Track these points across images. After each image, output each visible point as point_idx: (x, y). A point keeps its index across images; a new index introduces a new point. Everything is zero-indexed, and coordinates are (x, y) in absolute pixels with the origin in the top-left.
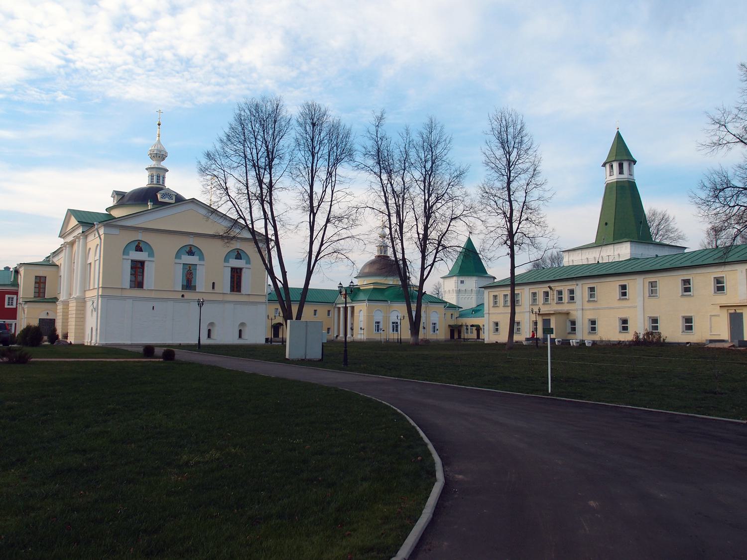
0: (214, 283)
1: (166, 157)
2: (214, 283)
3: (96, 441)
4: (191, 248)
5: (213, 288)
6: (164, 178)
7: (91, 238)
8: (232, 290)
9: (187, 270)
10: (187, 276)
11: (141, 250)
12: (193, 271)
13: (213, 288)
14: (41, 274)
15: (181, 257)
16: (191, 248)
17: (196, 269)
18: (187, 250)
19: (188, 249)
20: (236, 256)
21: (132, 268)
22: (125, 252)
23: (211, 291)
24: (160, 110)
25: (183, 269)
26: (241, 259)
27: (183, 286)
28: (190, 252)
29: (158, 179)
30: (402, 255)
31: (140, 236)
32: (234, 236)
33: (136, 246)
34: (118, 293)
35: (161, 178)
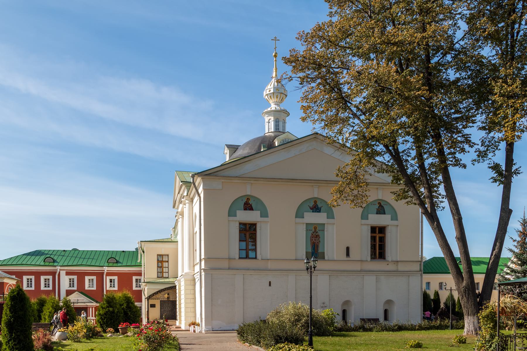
0: (348, 249)
2: (348, 249)
3: (388, 169)
4: (315, 202)
5: (348, 254)
6: (284, 122)
7: (515, 259)
8: (373, 256)
9: (311, 232)
10: (311, 240)
11: (251, 209)
12: (320, 233)
13: (348, 254)
15: (303, 214)
16: (315, 202)
17: (323, 230)
18: (311, 206)
19: (312, 204)
20: (377, 209)
21: (240, 231)
22: (231, 213)
23: (344, 257)
24: (275, 38)
25: (307, 230)
26: (385, 214)
27: (307, 253)
28: (315, 207)
30: (66, 265)
31: (248, 190)
32: (277, 342)
33: (245, 204)
34: (226, 264)
35: (281, 124)
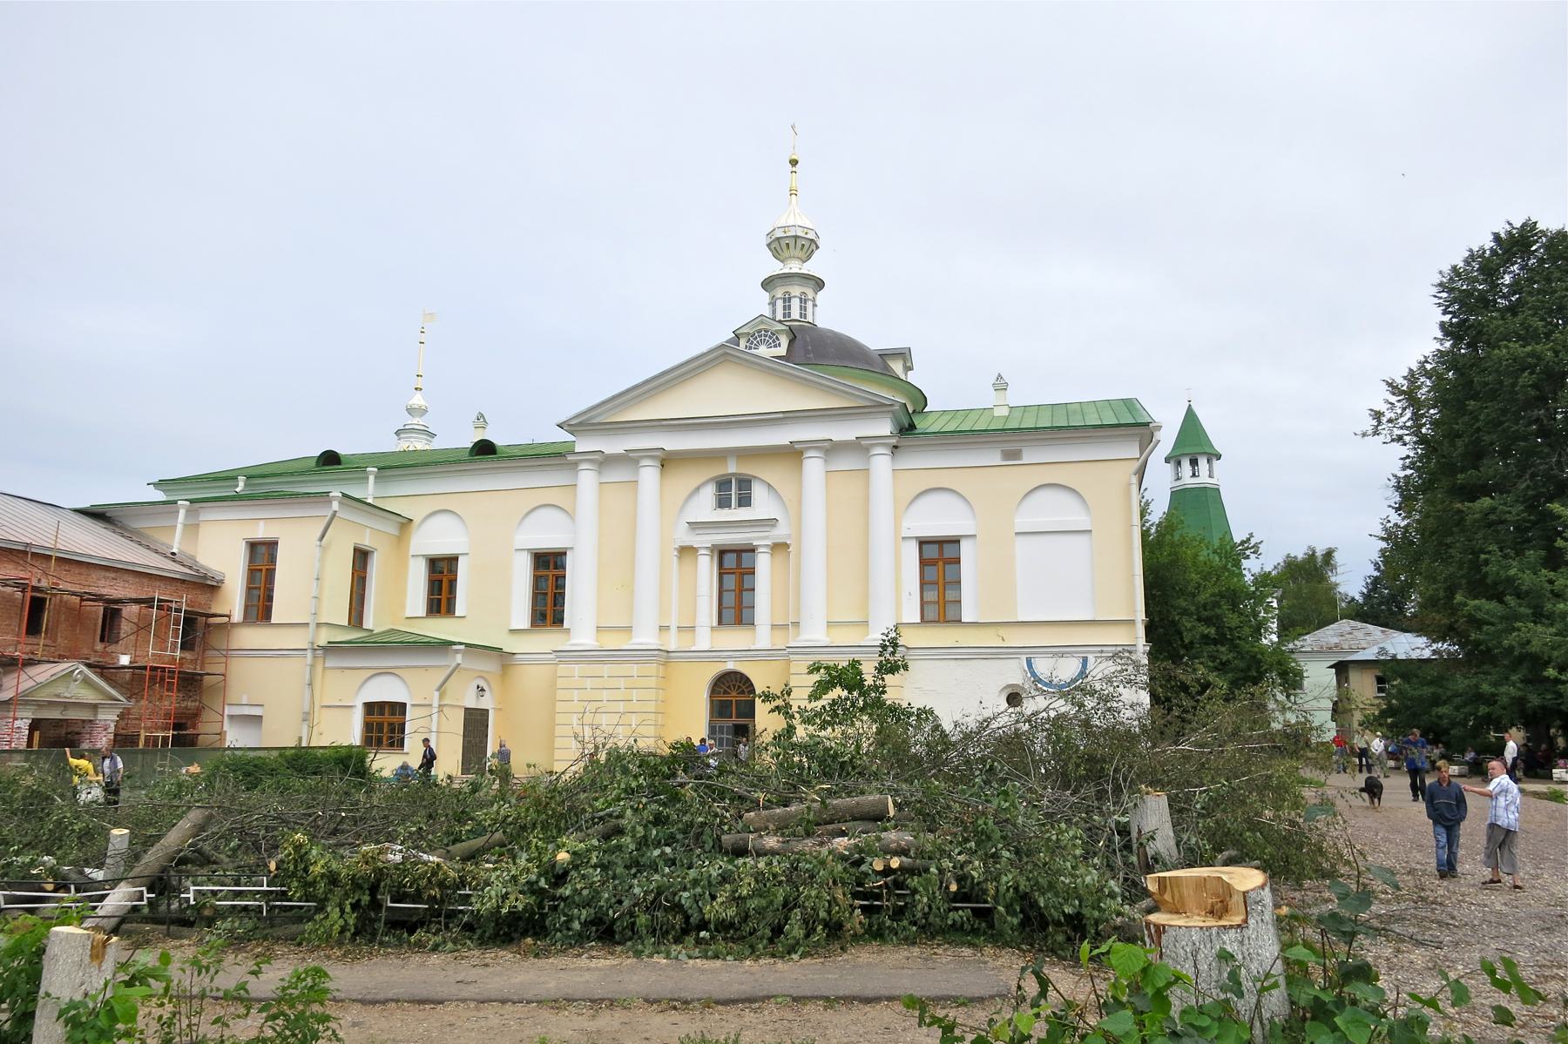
1: (817, 247)
14: (261, 532)
29: (803, 308)
35: (810, 304)
